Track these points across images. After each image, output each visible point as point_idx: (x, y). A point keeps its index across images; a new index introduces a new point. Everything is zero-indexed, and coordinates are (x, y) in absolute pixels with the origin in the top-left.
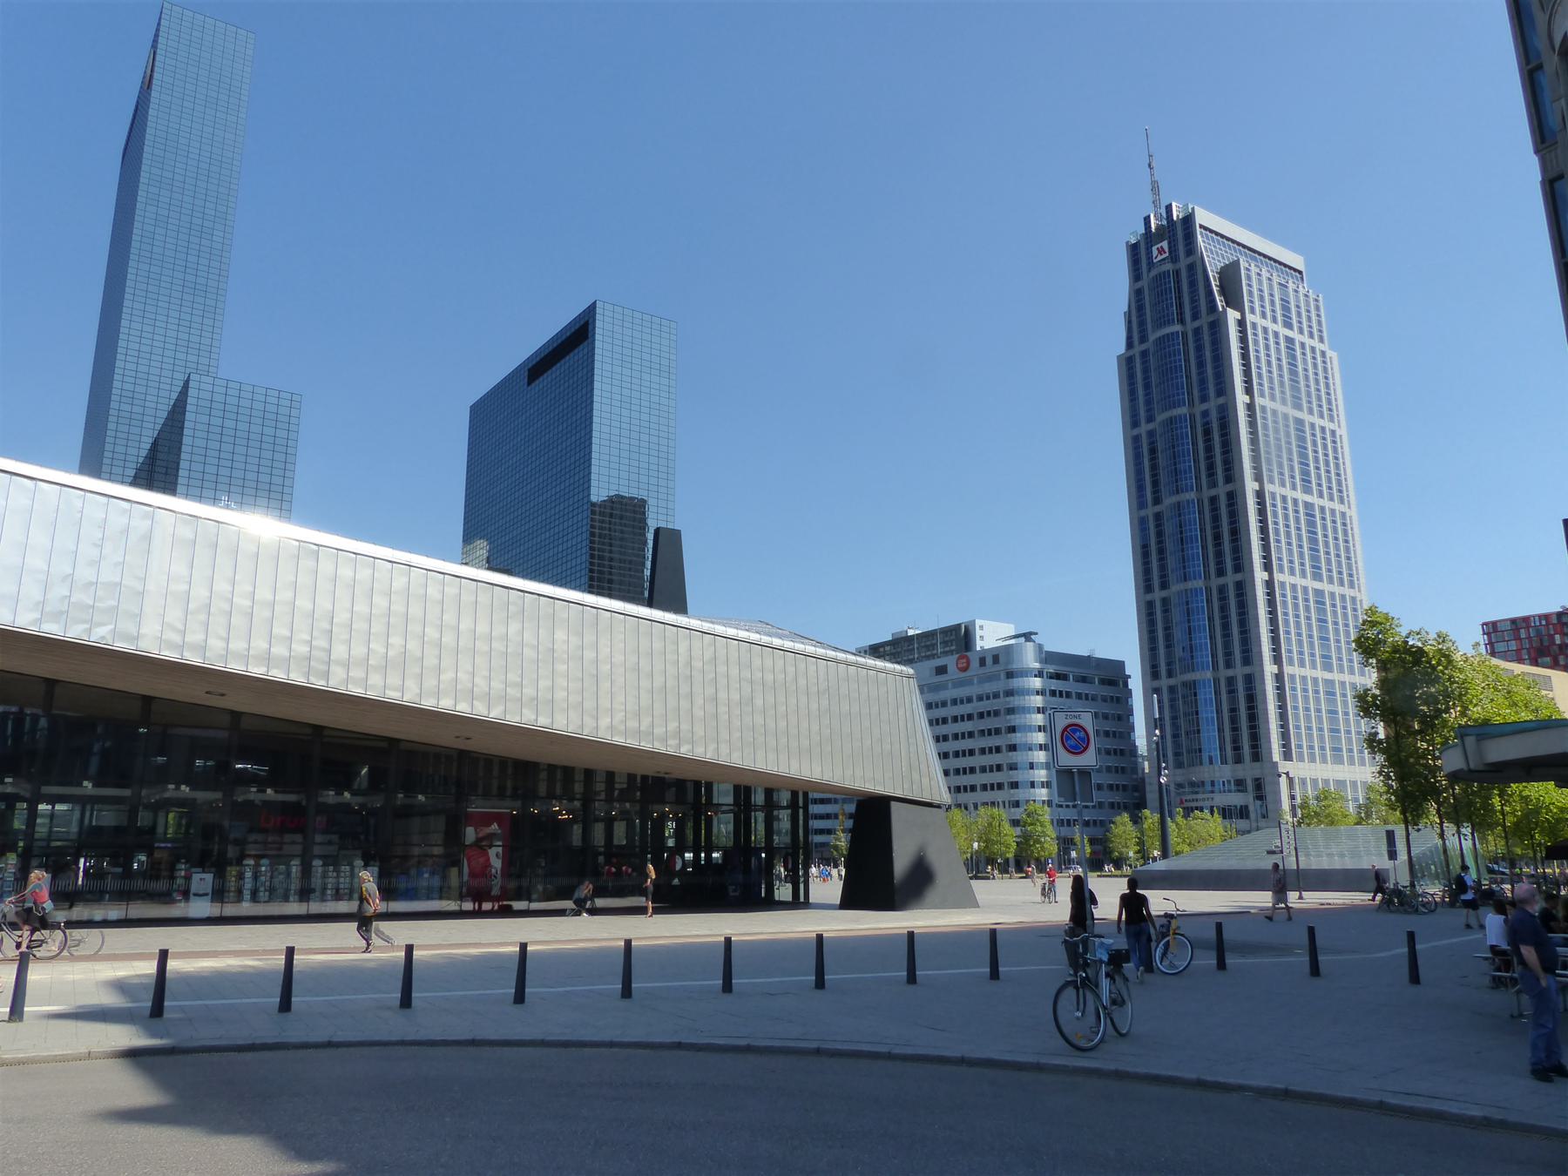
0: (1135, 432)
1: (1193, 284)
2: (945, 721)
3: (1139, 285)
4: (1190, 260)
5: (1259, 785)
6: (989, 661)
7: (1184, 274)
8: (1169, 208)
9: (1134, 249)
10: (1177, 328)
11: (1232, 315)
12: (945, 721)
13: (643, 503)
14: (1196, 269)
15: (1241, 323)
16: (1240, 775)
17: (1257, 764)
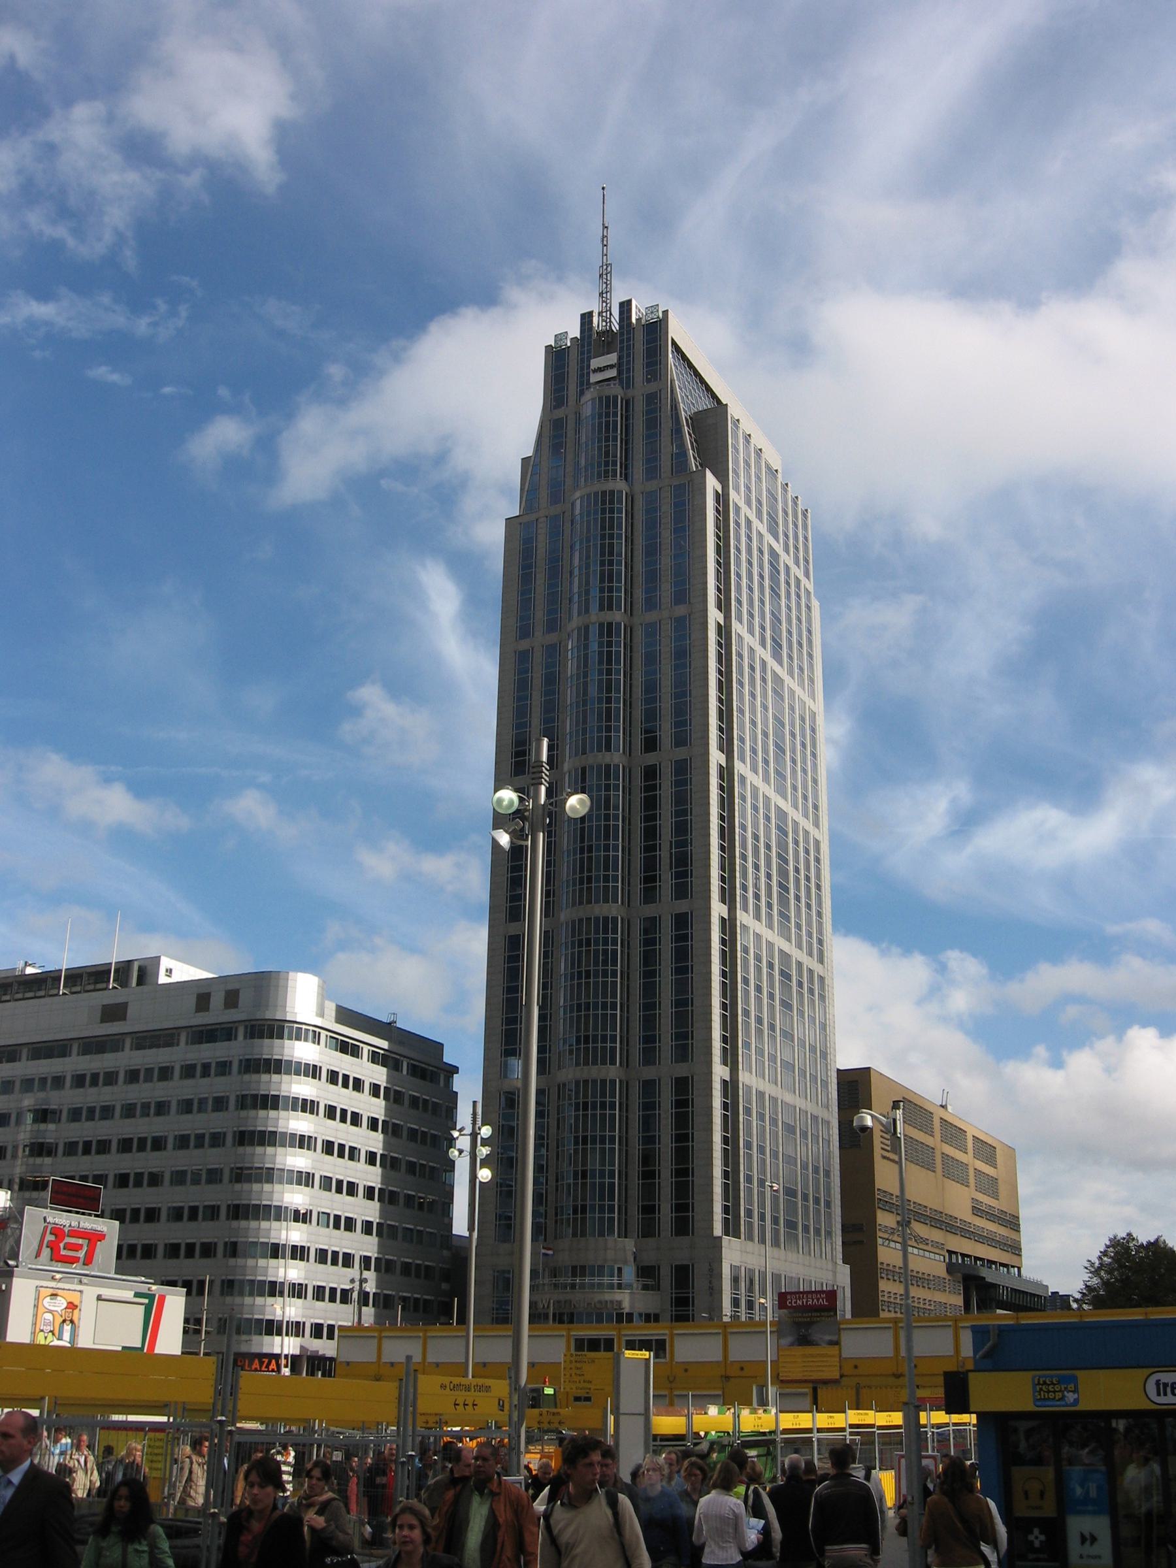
0: (524, 645)
1: (652, 423)
2: (152, 1215)
3: (559, 413)
4: (652, 387)
5: (683, 1274)
6: (217, 1001)
7: (639, 407)
8: (626, 307)
9: (557, 357)
10: (620, 485)
11: (712, 483)
12: (152, 1215)
13: (124, 1019)
14: (658, 403)
15: (722, 499)
16: (649, 1259)
17: (684, 1240)
